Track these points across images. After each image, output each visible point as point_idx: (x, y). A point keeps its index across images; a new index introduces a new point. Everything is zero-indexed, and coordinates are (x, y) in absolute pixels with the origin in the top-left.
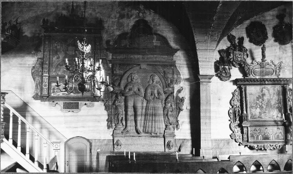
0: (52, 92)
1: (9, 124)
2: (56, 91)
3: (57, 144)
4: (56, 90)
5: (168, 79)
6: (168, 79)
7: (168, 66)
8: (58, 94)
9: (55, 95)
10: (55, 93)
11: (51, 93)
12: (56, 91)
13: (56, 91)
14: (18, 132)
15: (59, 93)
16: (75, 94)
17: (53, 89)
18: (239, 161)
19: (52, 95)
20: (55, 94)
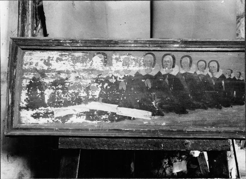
0: (24, 104)
1: (204, 156)
2: (47, 98)
3: (188, 54)
4: (48, 93)
5: (75, 67)
6: (75, 67)
7: (223, 132)
8: (60, 112)
9: (42, 121)
10: (42, 110)
11: (21, 108)
12: (52, 98)
13: (47, 98)
14: (205, 157)
15: (69, 110)
16: (159, 114)
17: (28, 87)
18: (232, 71)
19: (23, 120)
20: (46, 115)
